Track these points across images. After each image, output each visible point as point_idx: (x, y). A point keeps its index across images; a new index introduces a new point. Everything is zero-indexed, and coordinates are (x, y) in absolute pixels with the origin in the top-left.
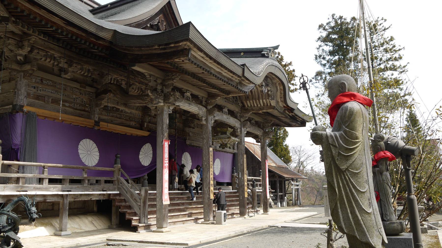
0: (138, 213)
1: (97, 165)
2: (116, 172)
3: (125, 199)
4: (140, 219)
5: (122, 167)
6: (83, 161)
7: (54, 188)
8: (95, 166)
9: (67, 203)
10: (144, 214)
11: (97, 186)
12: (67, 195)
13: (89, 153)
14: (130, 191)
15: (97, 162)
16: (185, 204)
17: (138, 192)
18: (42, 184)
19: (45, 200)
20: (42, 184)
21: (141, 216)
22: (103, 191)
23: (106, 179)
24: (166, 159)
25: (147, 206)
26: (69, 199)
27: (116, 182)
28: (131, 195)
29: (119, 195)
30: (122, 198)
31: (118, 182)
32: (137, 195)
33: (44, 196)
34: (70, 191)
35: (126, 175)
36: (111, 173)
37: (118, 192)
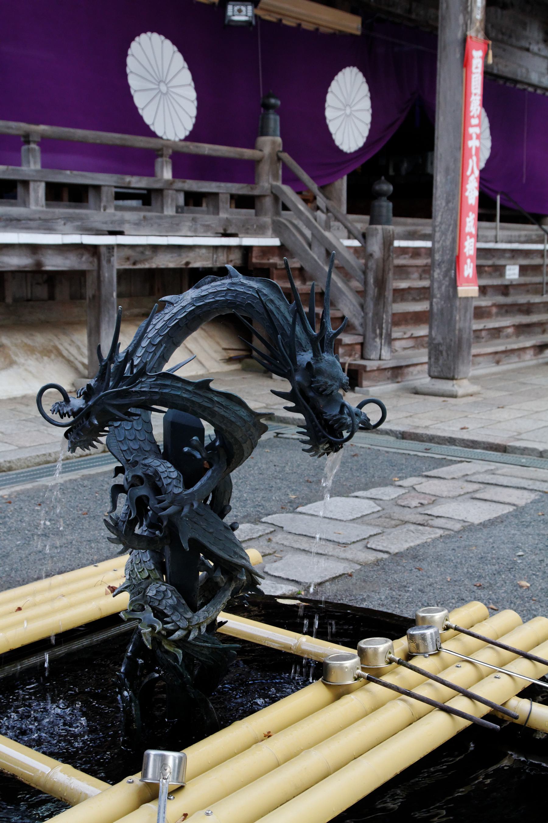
0: (357, 322)
1: (192, 137)
2: (265, 169)
3: (301, 270)
4: (362, 344)
5: (285, 149)
6: (148, 120)
7: (68, 219)
8: (187, 139)
9: (111, 276)
10: (378, 320)
11: (203, 215)
12: (110, 248)
13: (163, 88)
14: (323, 240)
15: (190, 127)
16: (489, 291)
17: (356, 243)
18: (25, 204)
19: (39, 264)
20: (25, 204)
21: (370, 334)
22: (225, 235)
23: (234, 191)
24: (474, 121)
25: (389, 295)
26: (118, 263)
27: (268, 202)
28: (328, 253)
29: (282, 250)
30: (294, 263)
31: (276, 198)
32: (350, 257)
33: (34, 249)
34: (121, 233)
35: (305, 177)
36: (246, 171)
37: (275, 242)
